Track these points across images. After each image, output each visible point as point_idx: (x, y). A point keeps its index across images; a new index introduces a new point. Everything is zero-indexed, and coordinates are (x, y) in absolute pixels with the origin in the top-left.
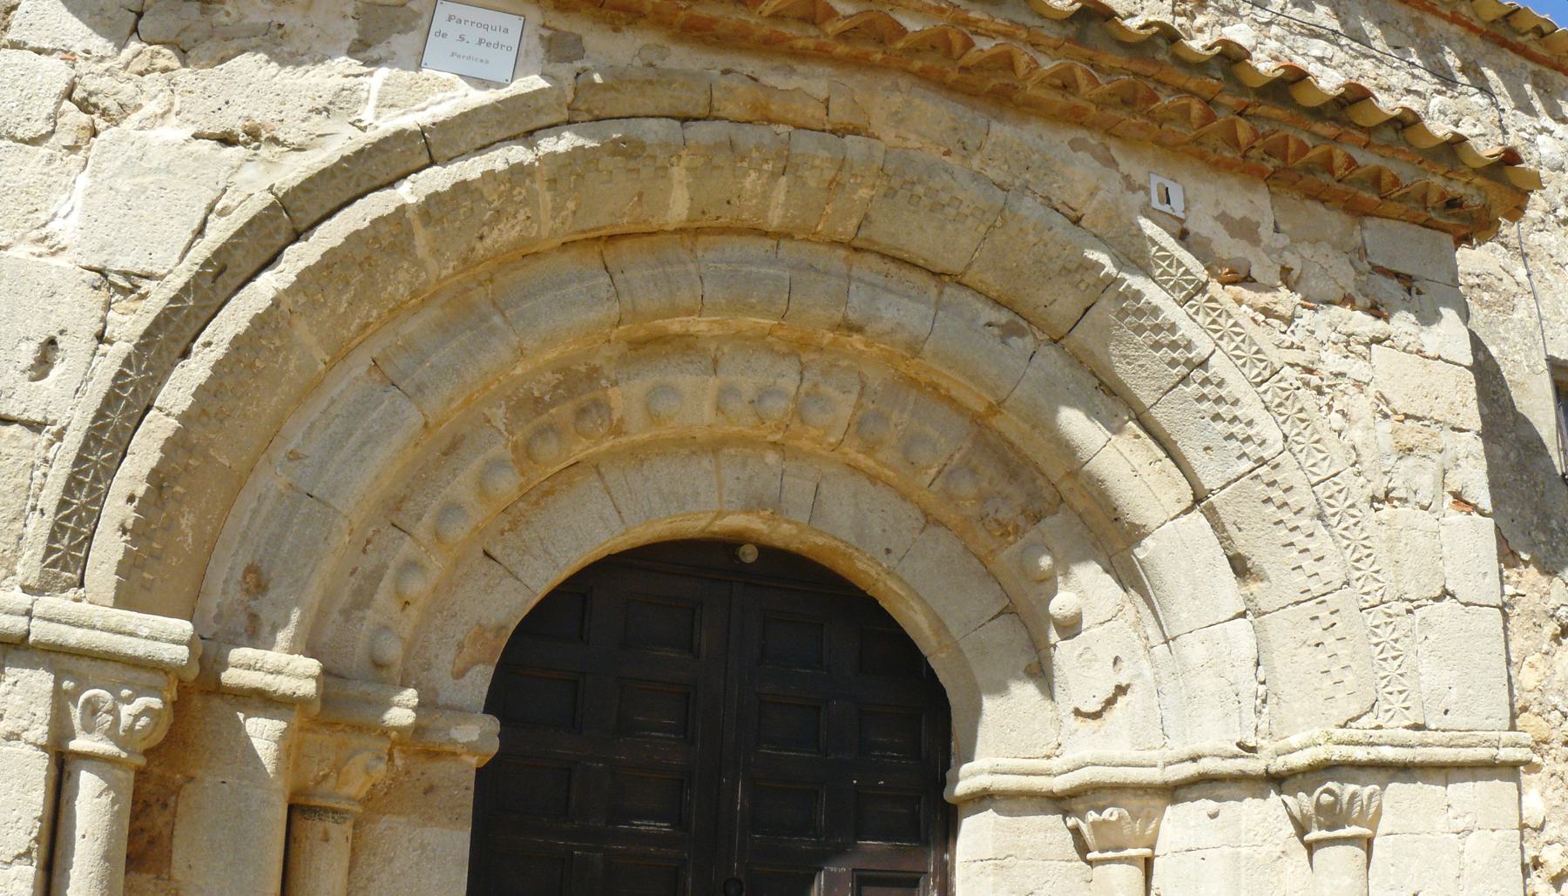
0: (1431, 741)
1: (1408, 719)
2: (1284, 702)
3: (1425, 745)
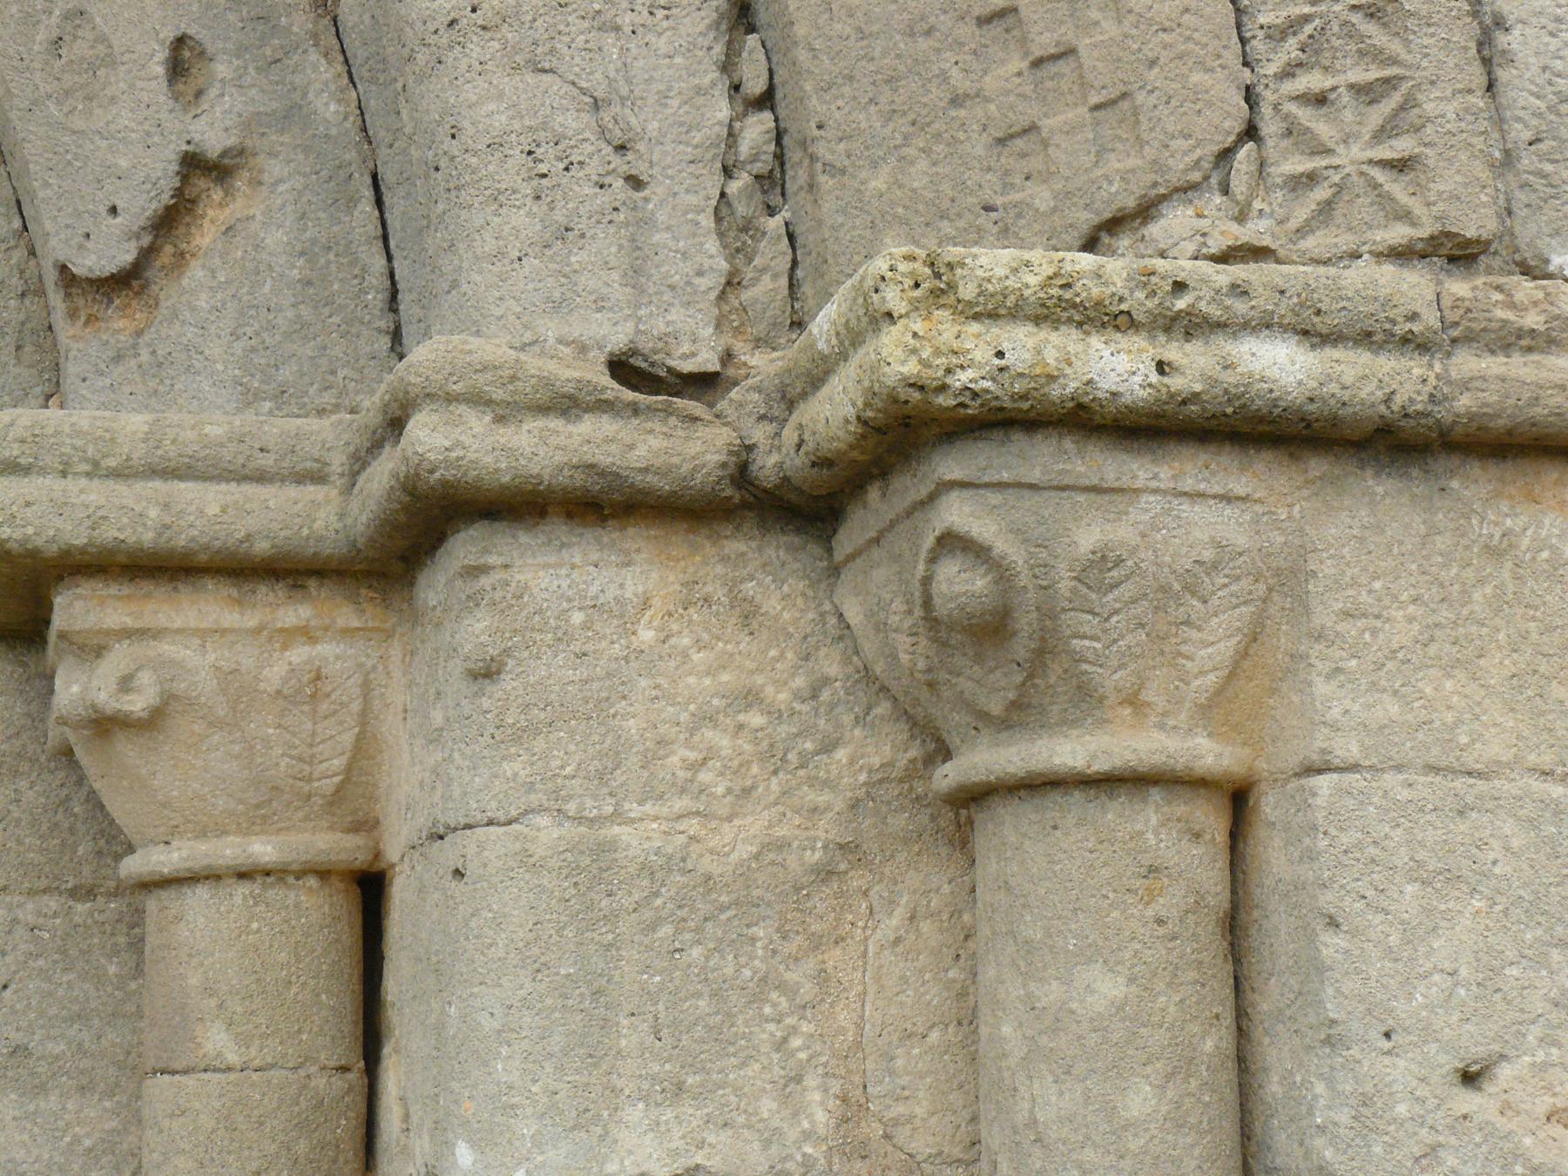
0: (1533, 320)
1: (1405, 216)
2: (829, 168)
3: (1510, 340)
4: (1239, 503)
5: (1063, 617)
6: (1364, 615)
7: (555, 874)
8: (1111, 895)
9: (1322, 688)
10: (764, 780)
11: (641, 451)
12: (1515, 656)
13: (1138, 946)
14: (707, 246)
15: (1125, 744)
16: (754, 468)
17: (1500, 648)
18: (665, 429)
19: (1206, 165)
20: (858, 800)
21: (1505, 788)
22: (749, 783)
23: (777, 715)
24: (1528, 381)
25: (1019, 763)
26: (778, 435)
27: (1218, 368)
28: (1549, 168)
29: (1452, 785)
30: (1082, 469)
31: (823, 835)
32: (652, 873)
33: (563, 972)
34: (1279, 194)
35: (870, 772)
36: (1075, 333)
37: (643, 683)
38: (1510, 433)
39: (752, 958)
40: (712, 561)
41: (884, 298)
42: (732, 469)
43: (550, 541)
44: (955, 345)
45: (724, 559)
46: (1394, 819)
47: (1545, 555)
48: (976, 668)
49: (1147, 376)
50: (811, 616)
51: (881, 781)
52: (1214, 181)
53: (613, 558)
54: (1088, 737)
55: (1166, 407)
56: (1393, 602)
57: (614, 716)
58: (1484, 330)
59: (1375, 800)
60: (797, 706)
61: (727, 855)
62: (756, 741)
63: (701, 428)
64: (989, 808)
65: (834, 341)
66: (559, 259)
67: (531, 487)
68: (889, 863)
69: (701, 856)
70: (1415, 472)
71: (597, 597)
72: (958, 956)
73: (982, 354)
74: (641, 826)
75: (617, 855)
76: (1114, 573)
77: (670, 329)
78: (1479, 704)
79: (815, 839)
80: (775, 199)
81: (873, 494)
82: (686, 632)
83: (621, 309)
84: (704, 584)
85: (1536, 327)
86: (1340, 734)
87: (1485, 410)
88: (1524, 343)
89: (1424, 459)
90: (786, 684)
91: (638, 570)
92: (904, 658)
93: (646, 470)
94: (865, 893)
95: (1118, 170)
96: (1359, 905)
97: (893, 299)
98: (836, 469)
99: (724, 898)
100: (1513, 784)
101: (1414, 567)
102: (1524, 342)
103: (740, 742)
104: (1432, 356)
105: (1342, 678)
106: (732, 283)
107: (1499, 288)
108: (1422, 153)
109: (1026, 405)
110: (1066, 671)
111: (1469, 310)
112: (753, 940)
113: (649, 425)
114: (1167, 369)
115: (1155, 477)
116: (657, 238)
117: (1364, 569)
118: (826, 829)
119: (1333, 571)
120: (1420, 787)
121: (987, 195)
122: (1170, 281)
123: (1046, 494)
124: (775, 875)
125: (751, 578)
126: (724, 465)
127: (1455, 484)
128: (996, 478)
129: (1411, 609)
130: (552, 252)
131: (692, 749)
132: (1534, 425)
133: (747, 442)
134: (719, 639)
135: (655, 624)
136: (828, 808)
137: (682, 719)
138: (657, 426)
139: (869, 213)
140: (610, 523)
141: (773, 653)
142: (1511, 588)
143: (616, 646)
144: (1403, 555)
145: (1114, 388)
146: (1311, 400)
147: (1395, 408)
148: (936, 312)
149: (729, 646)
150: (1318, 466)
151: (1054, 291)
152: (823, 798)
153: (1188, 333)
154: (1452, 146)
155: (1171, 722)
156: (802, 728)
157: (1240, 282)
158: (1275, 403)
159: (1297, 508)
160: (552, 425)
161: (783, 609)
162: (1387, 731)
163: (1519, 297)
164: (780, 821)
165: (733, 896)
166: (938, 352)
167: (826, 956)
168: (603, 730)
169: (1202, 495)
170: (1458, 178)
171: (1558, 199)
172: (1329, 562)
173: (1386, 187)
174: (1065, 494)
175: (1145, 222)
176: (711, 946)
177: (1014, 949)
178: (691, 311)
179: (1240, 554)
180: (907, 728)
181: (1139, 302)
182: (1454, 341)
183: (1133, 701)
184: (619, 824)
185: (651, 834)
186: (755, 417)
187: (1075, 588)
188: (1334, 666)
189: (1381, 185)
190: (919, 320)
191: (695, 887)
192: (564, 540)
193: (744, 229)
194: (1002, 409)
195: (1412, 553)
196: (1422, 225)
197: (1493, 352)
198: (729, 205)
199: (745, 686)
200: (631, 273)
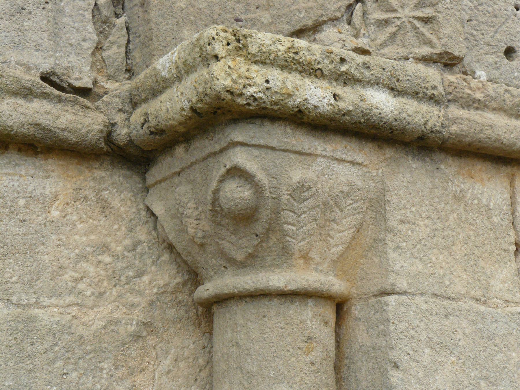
0: (478, 95)
1: (429, 43)
4: (358, 166)
5: (282, 213)
6: (409, 223)
7: (5, 332)
8: (291, 350)
9: (392, 255)
10: (110, 289)
11: (63, 120)
12: (466, 246)
13: (303, 375)
14: (88, 27)
15: (303, 277)
16: (115, 134)
17: (460, 242)
18: (73, 111)
19: (343, 10)
20: (153, 301)
21: (463, 306)
22: (103, 290)
23: (116, 257)
24: (479, 122)
25: (251, 284)
26: (128, 119)
27: (359, 100)
28: (475, 33)
29: (442, 303)
30: (295, 142)
31: (136, 318)
32: (54, 334)
33: (7, 384)
34: (372, 28)
35: (158, 288)
36: (298, 76)
37: (54, 237)
38: (469, 145)
39: (101, 378)
40: (89, 179)
41: (214, 48)
42: (104, 134)
43: (10, 162)
44: (247, 74)
45: (94, 179)
46: (421, 318)
47: (476, 202)
48: (233, 236)
49: (330, 100)
50: (134, 210)
51: (163, 293)
52: (345, 18)
53: (41, 173)
54: (284, 273)
55: (337, 116)
56: (419, 217)
57: (38, 253)
58: (461, 97)
59: (413, 308)
60: (126, 254)
61: (90, 326)
62: (106, 270)
63: (91, 112)
64: (227, 306)
65: (174, 71)
66: (18, 23)
67: (7, 132)
68: (166, 333)
69: (78, 326)
70: (428, 159)
71: (32, 192)
72: (196, 379)
73: (260, 80)
74: (48, 310)
75: (36, 324)
76: (306, 194)
77: (69, 65)
78: (453, 266)
79: (133, 320)
80: (119, 11)
81: (180, 150)
82: (75, 213)
83: (48, 51)
84: (85, 190)
85: (480, 99)
86: (399, 277)
87: (462, 133)
88: (475, 105)
89: (431, 154)
90: (121, 242)
91: (53, 181)
92: (191, 231)
93: (65, 130)
94: (154, 348)
95: (304, 7)
96: (407, 358)
97: (219, 49)
98: (164, 136)
99: (89, 348)
100: (466, 304)
101: (427, 202)
102: (475, 105)
103: (99, 269)
104: (440, 107)
105: (400, 251)
106: (99, 48)
107: (465, 80)
108: (437, 15)
109: (276, 108)
110: (278, 240)
111: (456, 88)
112: (102, 369)
113: (66, 108)
114: (337, 98)
115: (325, 150)
116: (65, 20)
117: (408, 201)
118: (138, 315)
119: (397, 201)
120: (430, 303)
121: (237, 14)
122: (339, 57)
123: (278, 153)
124: (113, 337)
125: (107, 189)
126: (102, 131)
127: (442, 166)
128: (257, 143)
129: (426, 221)
130: (15, 19)
131: (76, 271)
132: (480, 142)
133: (112, 122)
134: (90, 218)
135: (60, 208)
136: (139, 305)
137: (71, 257)
138: (70, 109)
139: (176, 18)
140: (40, 156)
141: (116, 227)
142: (464, 216)
143: (40, 218)
144: (423, 196)
145: (316, 104)
146: (396, 120)
147: (428, 128)
148: (237, 58)
149: (95, 222)
150: (389, 152)
151: (291, 55)
152: (137, 300)
153: (345, 83)
154: (448, 14)
155: (320, 268)
156: (128, 264)
157: (366, 62)
158: (381, 120)
159: (380, 171)
160: (19, 102)
161: (121, 206)
162: (418, 277)
163: (472, 85)
164: (116, 310)
165: (93, 347)
166: (240, 77)
167: (136, 378)
168: (32, 260)
169: (343, 160)
170: (451, 29)
171: (478, 46)
172: (395, 197)
173: (421, 29)
174: (286, 154)
175: (314, 33)
176: (82, 372)
177: (241, 375)
178: (80, 58)
179: (359, 190)
180: (176, 267)
181: (326, 65)
182: (449, 101)
183: (306, 257)
184: (37, 308)
185: (54, 314)
186: (116, 110)
187: (289, 199)
188: (396, 245)
189: (418, 28)
190: (230, 60)
191: (75, 342)
192: (17, 162)
193: (105, 22)
194: (265, 108)
195: (427, 196)
196: (436, 48)
197: (463, 108)
198: (98, 9)
199: (102, 242)
200: (53, 35)
